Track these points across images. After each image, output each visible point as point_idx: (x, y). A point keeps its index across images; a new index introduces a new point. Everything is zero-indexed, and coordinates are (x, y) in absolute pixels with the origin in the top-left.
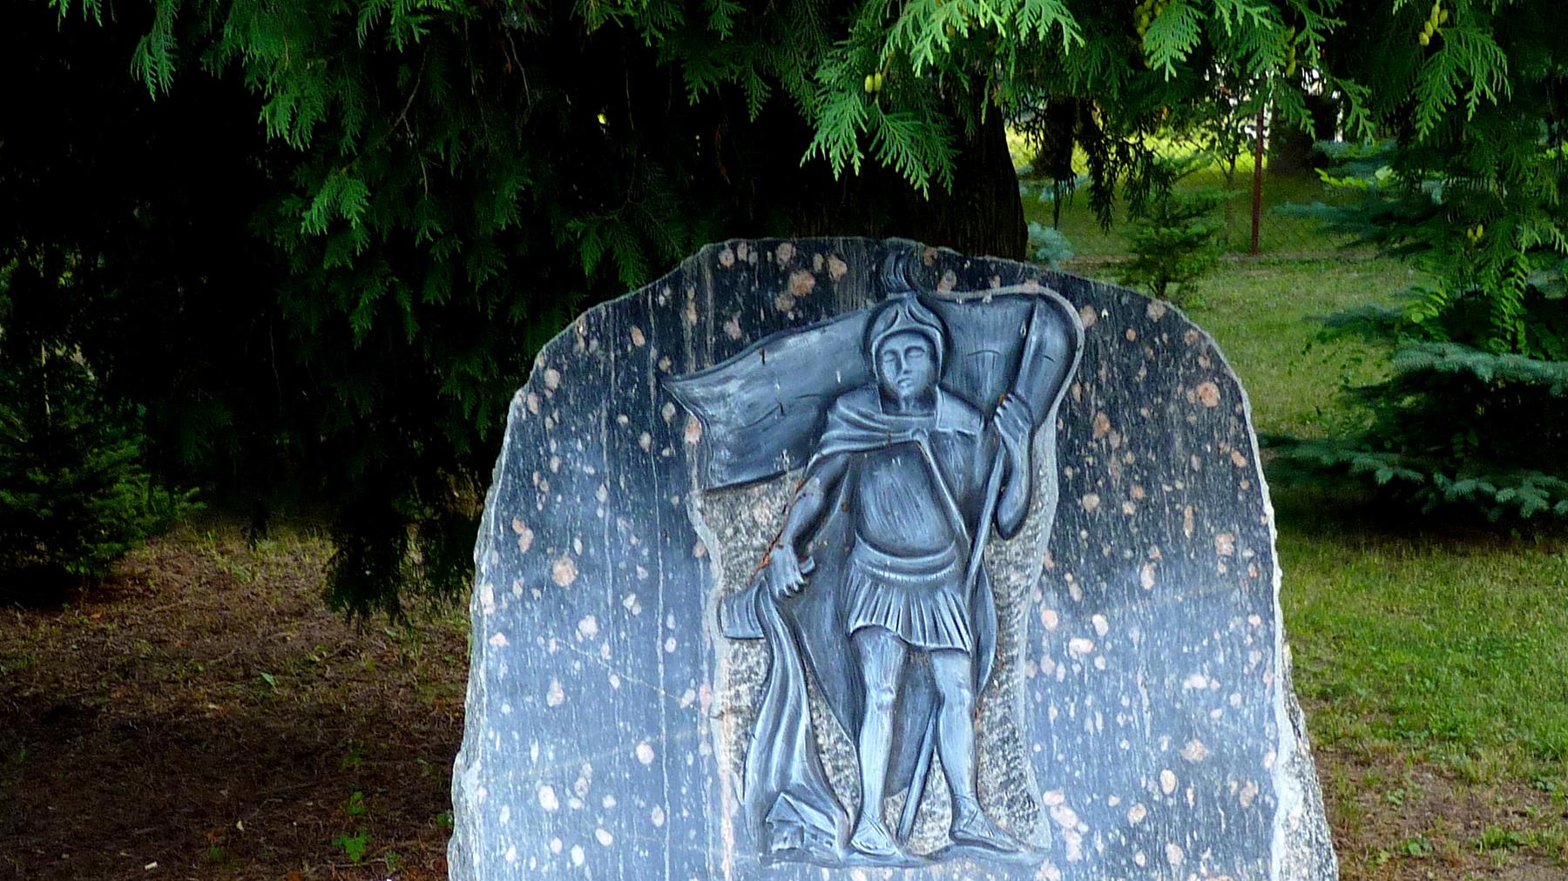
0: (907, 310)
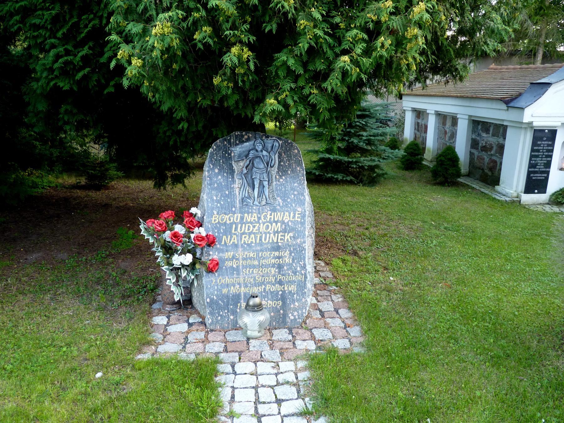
0: (259, 140)
